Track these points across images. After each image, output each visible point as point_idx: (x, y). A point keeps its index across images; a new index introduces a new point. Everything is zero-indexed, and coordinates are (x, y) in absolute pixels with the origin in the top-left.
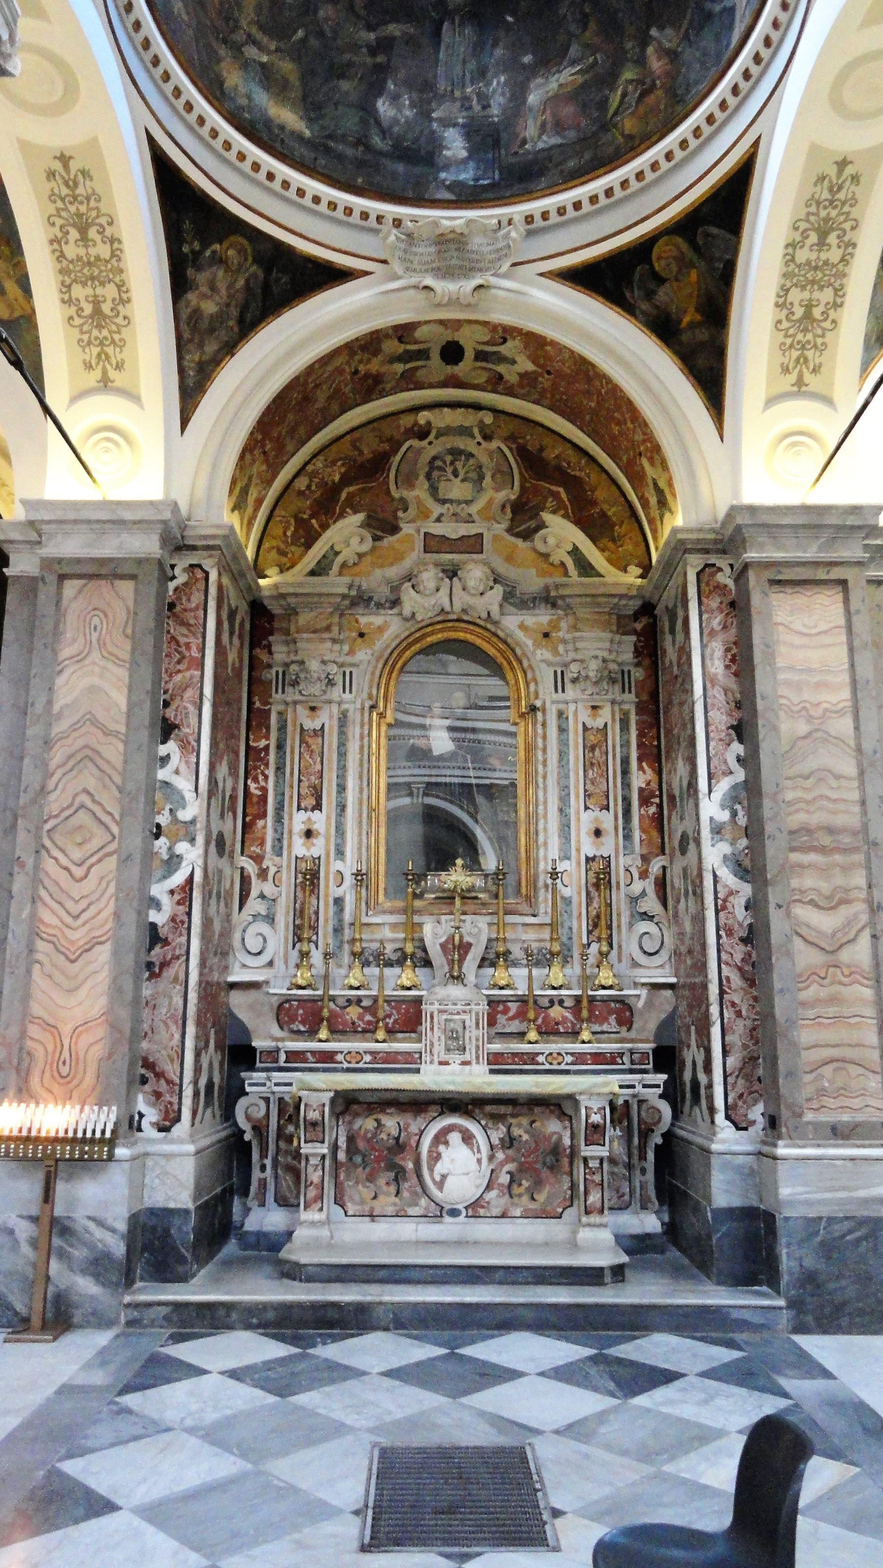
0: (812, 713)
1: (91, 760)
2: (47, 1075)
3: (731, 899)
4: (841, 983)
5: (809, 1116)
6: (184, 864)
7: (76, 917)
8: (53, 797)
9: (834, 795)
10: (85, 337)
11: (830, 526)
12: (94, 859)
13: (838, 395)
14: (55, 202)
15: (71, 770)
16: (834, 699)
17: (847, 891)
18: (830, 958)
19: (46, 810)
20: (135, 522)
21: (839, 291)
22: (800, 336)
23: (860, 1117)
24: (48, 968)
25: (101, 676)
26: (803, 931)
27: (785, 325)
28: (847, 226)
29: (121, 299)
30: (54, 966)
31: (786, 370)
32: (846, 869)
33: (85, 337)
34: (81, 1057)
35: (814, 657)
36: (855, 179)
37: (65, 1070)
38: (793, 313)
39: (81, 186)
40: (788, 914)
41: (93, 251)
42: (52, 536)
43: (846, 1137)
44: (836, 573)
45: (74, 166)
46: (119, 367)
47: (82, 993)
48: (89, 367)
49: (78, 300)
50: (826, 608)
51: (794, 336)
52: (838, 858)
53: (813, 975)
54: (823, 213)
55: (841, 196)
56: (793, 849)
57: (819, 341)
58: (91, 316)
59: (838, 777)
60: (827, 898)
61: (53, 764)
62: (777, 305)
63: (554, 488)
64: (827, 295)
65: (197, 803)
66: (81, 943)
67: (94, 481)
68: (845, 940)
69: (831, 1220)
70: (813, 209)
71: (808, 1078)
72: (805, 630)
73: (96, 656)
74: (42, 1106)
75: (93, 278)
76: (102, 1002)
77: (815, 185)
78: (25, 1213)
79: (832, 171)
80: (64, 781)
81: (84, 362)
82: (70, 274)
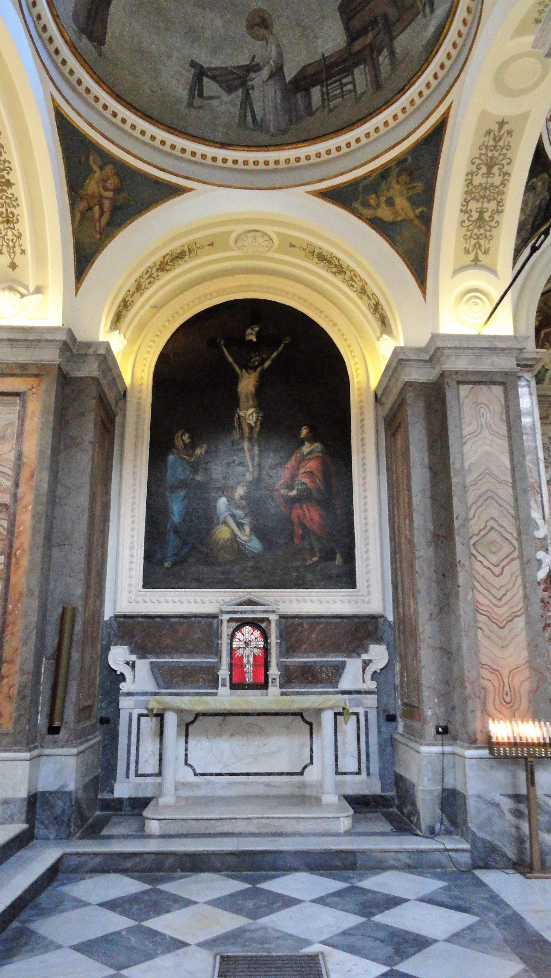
1: (492, 498)
2: (497, 702)
6: (543, 565)
7: (500, 600)
8: (473, 522)
12: (505, 563)
13: (500, 268)
15: (482, 505)
19: (470, 530)
20: (502, 349)
21: (500, 203)
24: (487, 633)
25: (491, 446)
27: (467, 223)
28: (505, 162)
30: (491, 631)
31: (467, 252)
33: (469, 233)
34: (517, 690)
36: (509, 133)
37: (508, 699)
39: (472, 244)
42: (449, 357)
47: (511, 648)
51: (501, 154)
54: (490, 154)
55: (501, 143)
57: (488, 234)
61: (470, 501)
62: (461, 211)
64: (493, 205)
65: (546, 526)
66: (505, 616)
67: (486, 323)
70: (484, 151)
73: (485, 433)
74: (496, 722)
76: (524, 655)
77: (485, 136)
78: (504, 793)
79: (496, 127)
80: (478, 511)
81: (465, 249)
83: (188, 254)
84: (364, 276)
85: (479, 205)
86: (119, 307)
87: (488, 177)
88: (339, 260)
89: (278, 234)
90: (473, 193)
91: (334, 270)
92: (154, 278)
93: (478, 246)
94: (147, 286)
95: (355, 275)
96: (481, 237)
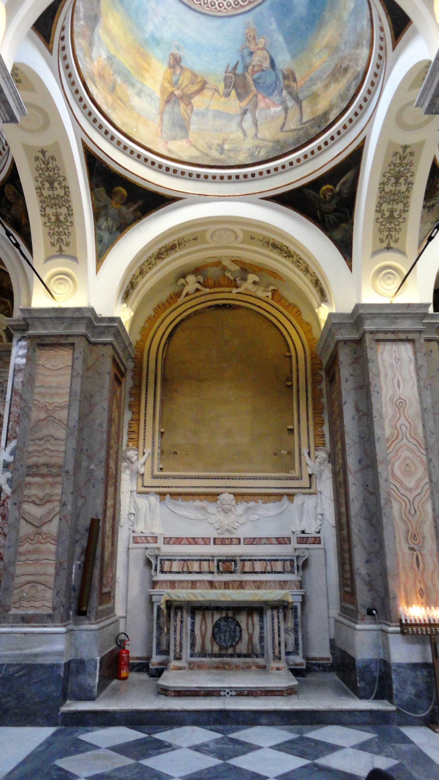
0: (49, 408)
3: (7, 500)
4: (41, 543)
5: (13, 611)
9: (52, 448)
10: (52, 232)
11: (69, 318)
13: (408, 250)
14: (69, 232)
16: (60, 401)
17: (51, 496)
18: (37, 530)
21: (406, 205)
22: (402, 169)
23: (38, 612)
26: (27, 517)
27: (48, 224)
28: (381, 220)
29: (41, 190)
31: (382, 241)
32: (53, 485)
33: (52, 232)
35: (54, 380)
36: (411, 154)
38: (384, 215)
40: (19, 509)
41: (56, 193)
43: (28, 622)
44: (70, 340)
45: (47, 155)
46: (67, 245)
48: (53, 245)
49: (48, 214)
50: (406, 351)
51: (405, 169)
52: (50, 479)
53: (28, 538)
55: (406, 161)
56: (28, 475)
57: (397, 227)
58: (55, 222)
59: (56, 439)
60: (41, 500)
62: (376, 211)
63: (5, 300)
64: (400, 206)
68: (46, 520)
69: (9, 666)
71: (16, 591)
72: (51, 367)
75: (55, 204)
77: (393, 156)
79: (401, 151)
81: (380, 239)
82: (45, 203)
83: (178, 246)
84: (306, 260)
85: (390, 206)
86: (128, 287)
87: (392, 209)
88: (287, 248)
89: (243, 231)
90: (403, 197)
91: (285, 255)
92: (153, 265)
93: (60, 240)
94: (148, 271)
95: (300, 258)
96: (392, 230)
